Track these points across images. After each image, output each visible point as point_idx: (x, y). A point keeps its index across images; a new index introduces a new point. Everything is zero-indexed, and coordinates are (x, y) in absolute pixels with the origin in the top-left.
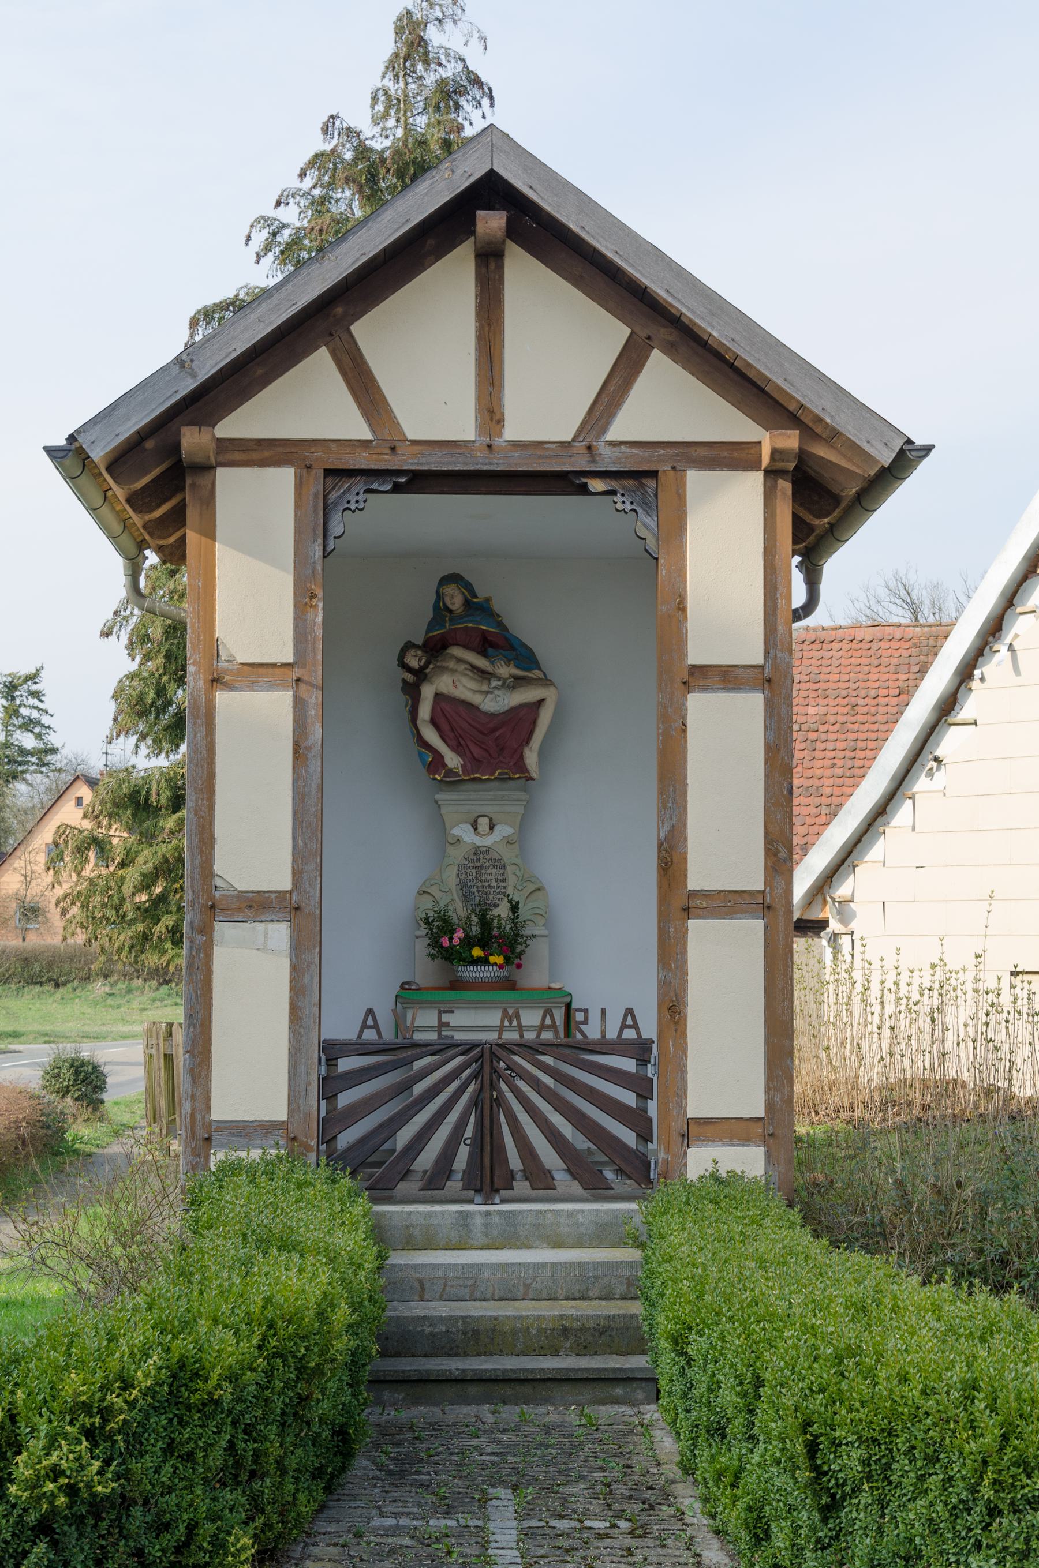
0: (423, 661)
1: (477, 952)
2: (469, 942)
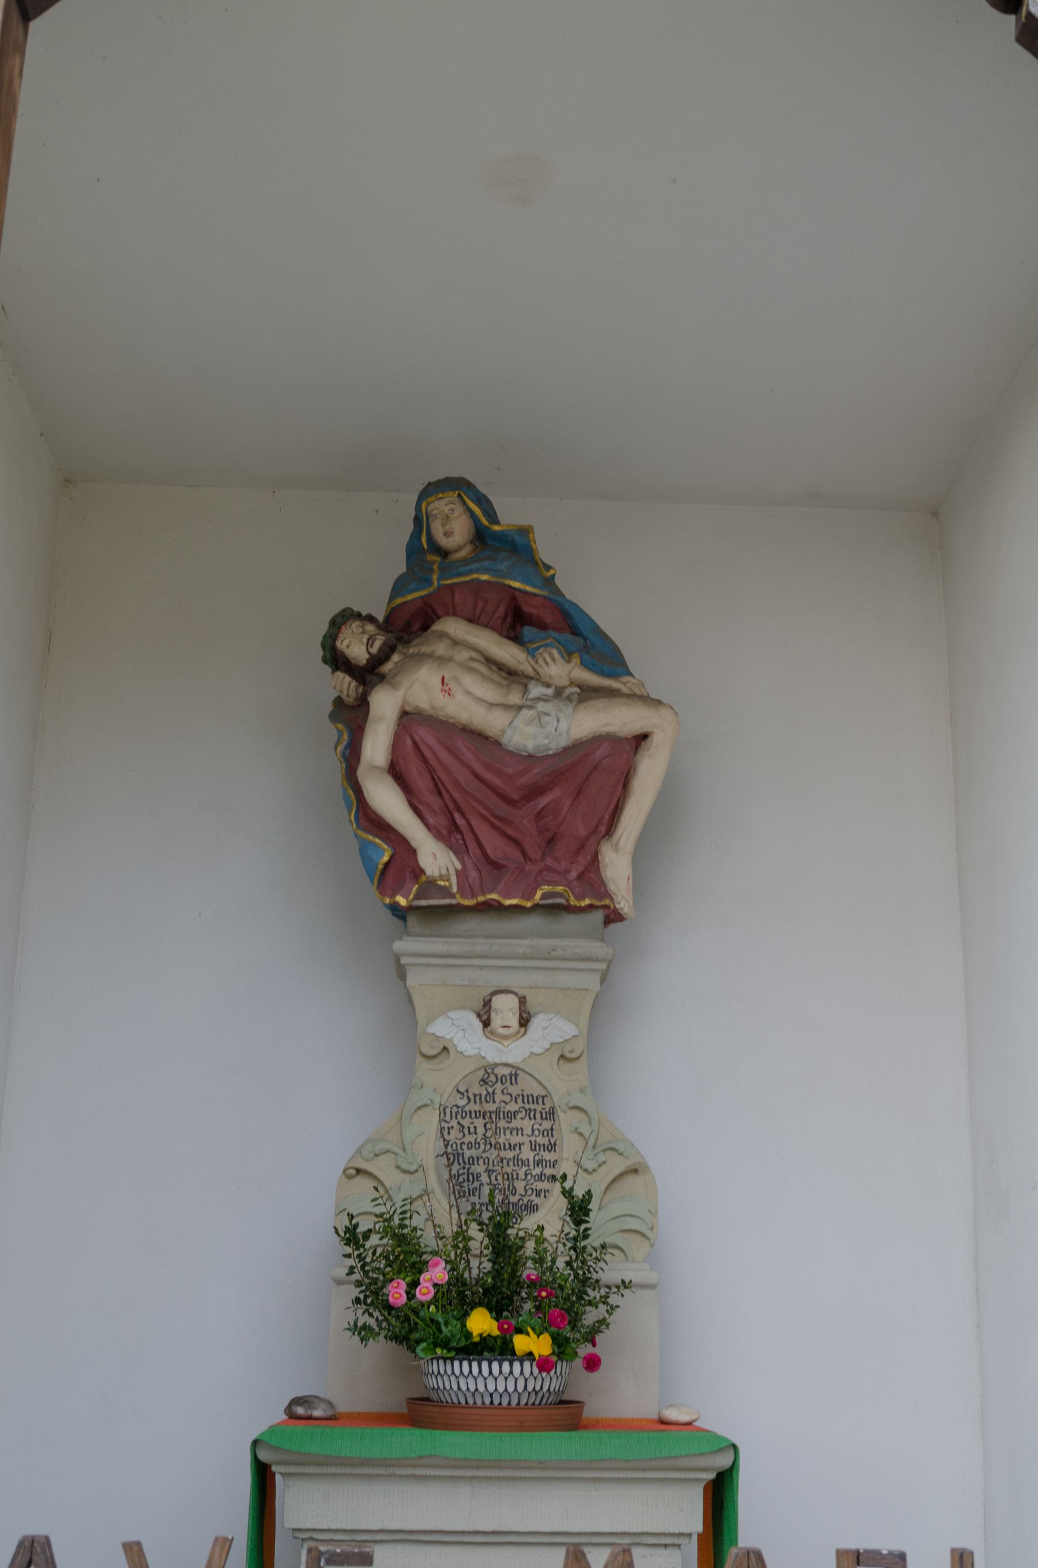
0: (378, 644)
1: (481, 1323)
2: (461, 1295)
